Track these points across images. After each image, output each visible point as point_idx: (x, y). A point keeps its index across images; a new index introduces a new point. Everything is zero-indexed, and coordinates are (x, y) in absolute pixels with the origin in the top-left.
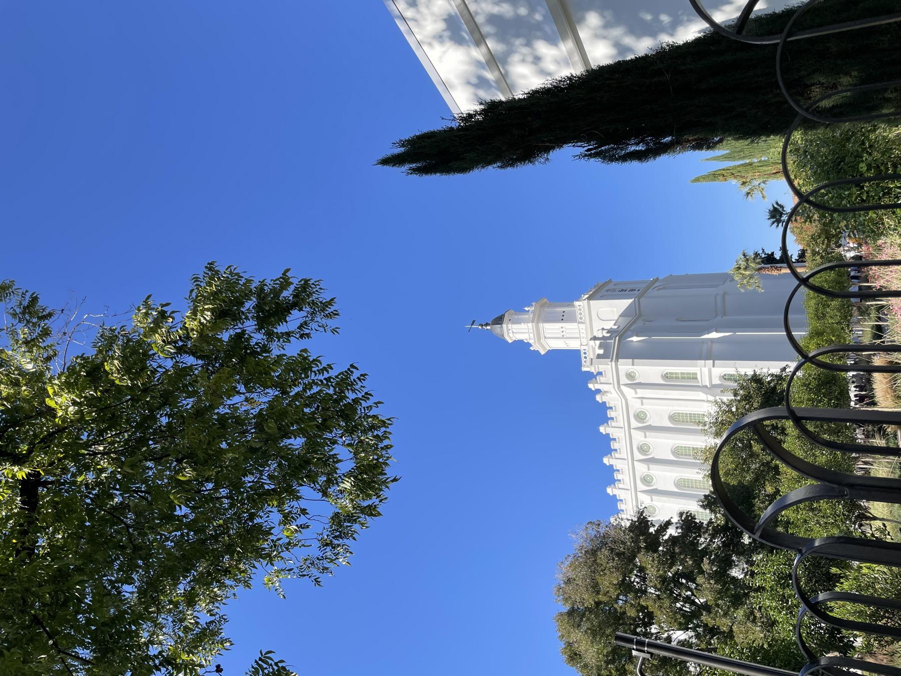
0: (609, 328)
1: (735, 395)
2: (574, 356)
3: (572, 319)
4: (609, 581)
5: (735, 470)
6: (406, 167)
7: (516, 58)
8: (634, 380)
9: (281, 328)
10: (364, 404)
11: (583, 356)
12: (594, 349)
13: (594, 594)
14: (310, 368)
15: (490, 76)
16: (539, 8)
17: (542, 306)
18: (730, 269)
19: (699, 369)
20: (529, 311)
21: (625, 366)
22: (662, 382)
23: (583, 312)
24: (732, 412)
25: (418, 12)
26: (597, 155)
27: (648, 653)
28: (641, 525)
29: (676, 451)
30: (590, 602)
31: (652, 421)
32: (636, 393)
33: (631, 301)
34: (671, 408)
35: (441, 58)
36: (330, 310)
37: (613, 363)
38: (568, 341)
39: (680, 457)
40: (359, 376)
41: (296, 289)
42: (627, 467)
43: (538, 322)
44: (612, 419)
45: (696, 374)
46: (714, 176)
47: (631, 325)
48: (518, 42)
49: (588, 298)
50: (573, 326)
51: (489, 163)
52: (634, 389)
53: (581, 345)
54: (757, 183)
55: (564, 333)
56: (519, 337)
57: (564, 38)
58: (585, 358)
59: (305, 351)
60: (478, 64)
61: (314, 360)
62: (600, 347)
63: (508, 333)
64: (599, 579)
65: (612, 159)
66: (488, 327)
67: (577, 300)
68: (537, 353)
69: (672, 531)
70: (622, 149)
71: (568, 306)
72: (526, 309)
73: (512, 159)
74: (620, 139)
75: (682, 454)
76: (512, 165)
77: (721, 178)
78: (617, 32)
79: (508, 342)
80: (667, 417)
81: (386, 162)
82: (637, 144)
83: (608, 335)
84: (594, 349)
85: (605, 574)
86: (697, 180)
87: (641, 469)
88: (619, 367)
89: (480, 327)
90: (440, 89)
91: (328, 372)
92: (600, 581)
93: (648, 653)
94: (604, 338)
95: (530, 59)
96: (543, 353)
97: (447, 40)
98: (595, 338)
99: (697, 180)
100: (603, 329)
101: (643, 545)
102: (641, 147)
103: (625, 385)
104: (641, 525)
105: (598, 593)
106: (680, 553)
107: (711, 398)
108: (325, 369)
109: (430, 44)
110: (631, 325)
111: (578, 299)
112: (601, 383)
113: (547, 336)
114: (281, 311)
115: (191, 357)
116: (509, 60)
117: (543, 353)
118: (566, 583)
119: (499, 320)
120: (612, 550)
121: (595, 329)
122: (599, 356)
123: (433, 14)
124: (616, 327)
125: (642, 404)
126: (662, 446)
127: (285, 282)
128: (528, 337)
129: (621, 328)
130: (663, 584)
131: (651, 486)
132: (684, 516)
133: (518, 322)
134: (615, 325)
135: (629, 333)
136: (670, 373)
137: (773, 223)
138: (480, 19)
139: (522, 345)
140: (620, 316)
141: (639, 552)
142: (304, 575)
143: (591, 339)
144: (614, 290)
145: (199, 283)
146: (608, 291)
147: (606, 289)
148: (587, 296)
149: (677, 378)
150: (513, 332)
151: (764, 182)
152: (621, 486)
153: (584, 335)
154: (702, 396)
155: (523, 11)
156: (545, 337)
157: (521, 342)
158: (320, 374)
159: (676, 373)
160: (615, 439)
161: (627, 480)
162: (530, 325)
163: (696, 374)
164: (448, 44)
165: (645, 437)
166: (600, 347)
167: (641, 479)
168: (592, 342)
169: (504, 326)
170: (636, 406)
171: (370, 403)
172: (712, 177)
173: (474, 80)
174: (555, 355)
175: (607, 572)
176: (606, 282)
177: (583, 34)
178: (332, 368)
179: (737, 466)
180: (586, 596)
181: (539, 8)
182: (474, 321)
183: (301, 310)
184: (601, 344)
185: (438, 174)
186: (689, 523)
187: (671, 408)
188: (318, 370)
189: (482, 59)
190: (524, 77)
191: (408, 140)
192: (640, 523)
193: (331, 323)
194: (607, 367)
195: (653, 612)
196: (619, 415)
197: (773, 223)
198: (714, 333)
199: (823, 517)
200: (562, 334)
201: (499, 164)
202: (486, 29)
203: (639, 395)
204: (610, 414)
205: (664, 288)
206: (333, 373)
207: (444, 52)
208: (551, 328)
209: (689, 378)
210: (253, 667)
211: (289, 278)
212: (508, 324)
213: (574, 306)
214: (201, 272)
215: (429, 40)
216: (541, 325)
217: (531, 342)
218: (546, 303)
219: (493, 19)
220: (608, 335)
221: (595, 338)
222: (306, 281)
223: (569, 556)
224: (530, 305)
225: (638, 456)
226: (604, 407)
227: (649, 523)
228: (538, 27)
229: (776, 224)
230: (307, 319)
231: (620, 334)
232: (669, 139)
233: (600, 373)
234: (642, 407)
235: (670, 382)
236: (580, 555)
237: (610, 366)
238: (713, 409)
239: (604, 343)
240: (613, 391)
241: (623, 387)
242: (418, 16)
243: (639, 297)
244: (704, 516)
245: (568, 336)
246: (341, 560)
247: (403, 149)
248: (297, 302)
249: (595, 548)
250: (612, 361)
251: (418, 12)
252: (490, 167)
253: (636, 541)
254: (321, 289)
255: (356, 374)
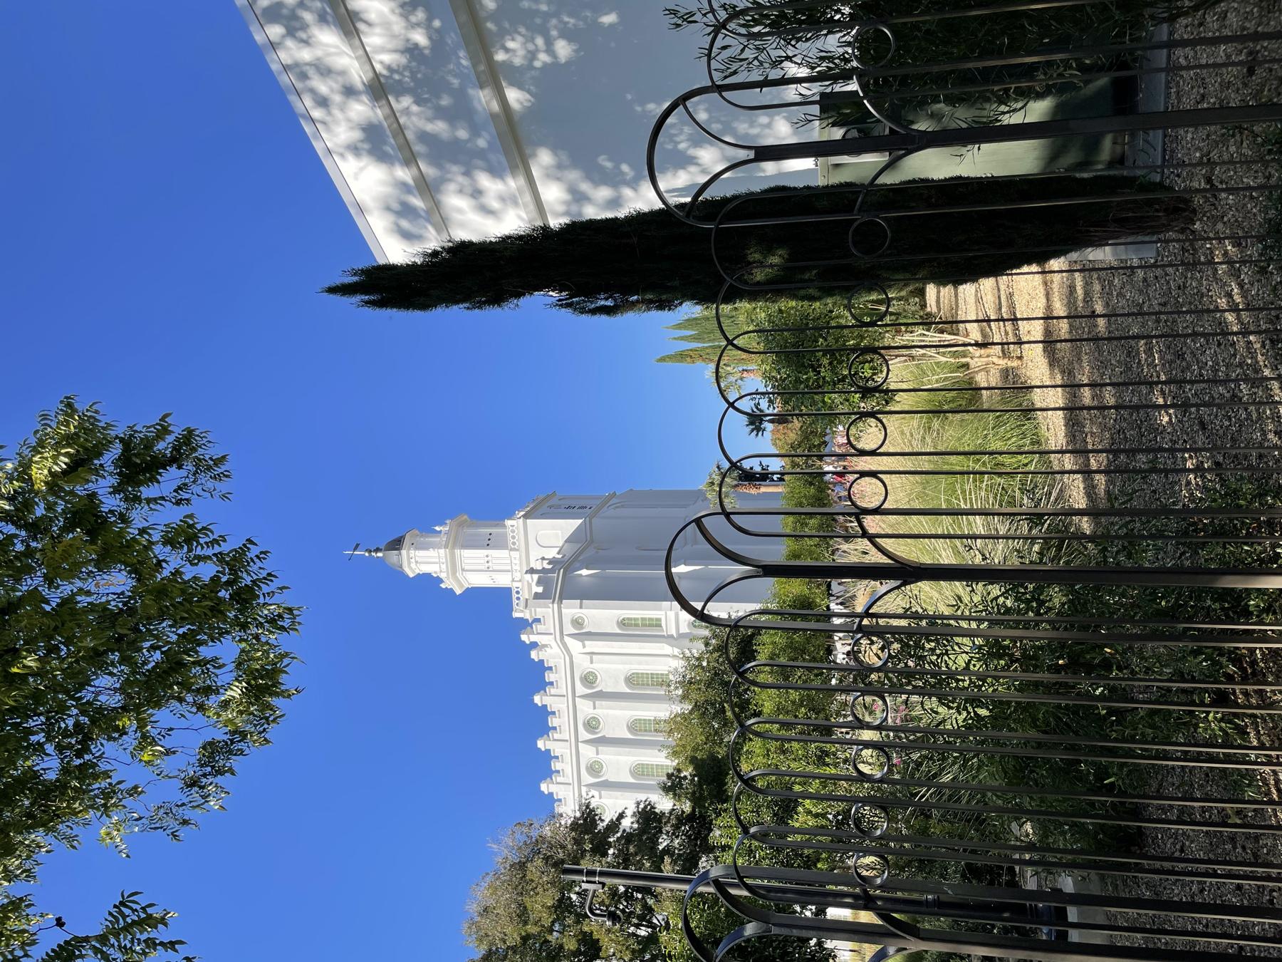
0: (551, 557)
1: (707, 644)
2: (501, 597)
3: (501, 544)
4: (541, 903)
5: (706, 744)
6: (358, 298)
7: (452, 187)
8: (582, 628)
9: (147, 492)
10: (265, 589)
11: (515, 596)
12: (530, 586)
13: (521, 925)
14: (195, 537)
15: (417, 202)
16: (484, 133)
17: (461, 525)
18: (702, 487)
19: (663, 613)
20: (440, 532)
21: (571, 609)
22: (618, 631)
23: (517, 528)
24: (703, 668)
25: (329, 113)
26: (569, 305)
27: (600, 883)
28: (588, 819)
29: (635, 726)
30: (514, 938)
31: (604, 685)
32: (584, 647)
33: (580, 521)
34: (628, 667)
35: (356, 176)
36: (220, 471)
37: (556, 605)
38: (495, 575)
39: (639, 733)
40: (258, 553)
41: (177, 439)
42: (568, 751)
43: (454, 547)
44: (551, 683)
45: (659, 620)
46: (682, 356)
47: (581, 553)
48: (455, 168)
49: (523, 516)
50: (503, 553)
51: (457, 302)
52: (582, 641)
53: (513, 580)
54: (734, 379)
55: (490, 564)
56: (425, 569)
57: (513, 169)
58: (518, 598)
59: (191, 516)
60: (403, 186)
61: (204, 528)
62: (539, 583)
63: (409, 563)
64: (528, 901)
65: (583, 311)
66: (380, 554)
67: (510, 518)
68: (450, 592)
69: (627, 823)
70: (592, 302)
71: (496, 526)
72: (437, 528)
73: (479, 302)
74: (589, 291)
75: (640, 730)
76: (480, 307)
77: (689, 359)
78: (573, 175)
79: (408, 576)
80: (623, 678)
81: (332, 290)
82: (606, 299)
83: (550, 567)
84: (530, 586)
85: (537, 894)
86: (662, 359)
87: (588, 752)
88: (564, 611)
89: (367, 554)
90: (352, 211)
91: (219, 545)
92: (528, 905)
93: (600, 883)
94: (544, 571)
95: (469, 190)
96: (458, 592)
97: (364, 153)
98: (532, 571)
99: (662, 359)
100: (543, 559)
101: (588, 847)
102: (610, 303)
103: (569, 635)
104: (588, 819)
105: (526, 923)
106: (636, 854)
107: (676, 651)
108: (215, 542)
109: (342, 155)
110: (581, 553)
111: (510, 516)
112: (538, 634)
113: (466, 568)
114: (153, 467)
115: (10, 526)
116: (442, 188)
117: (458, 592)
118: (481, 915)
119: (396, 544)
120: (546, 859)
121: (532, 559)
122: (537, 596)
123: (349, 120)
124: (560, 556)
125: (592, 662)
126: (616, 718)
127: (164, 431)
128: (438, 570)
129: (568, 556)
130: (613, 898)
131: (599, 777)
132: (642, 806)
133: (425, 547)
134: (558, 553)
135: (578, 565)
136: (628, 619)
137: (752, 431)
138: (410, 135)
139: (429, 582)
140: (566, 541)
141: (583, 857)
142: (156, 828)
143: (526, 573)
144: (559, 507)
145: (48, 422)
146: (550, 507)
147: (549, 504)
148: (522, 513)
149: (636, 625)
150: (417, 562)
151: (742, 379)
152: (560, 779)
153: (518, 568)
154: (667, 649)
155: (462, 134)
156: (463, 570)
157: (427, 576)
158: (208, 547)
159: (635, 619)
160: (554, 713)
161: (568, 770)
162: (442, 551)
163: (659, 620)
164: (365, 161)
165: (595, 708)
166: (539, 583)
167: (587, 768)
168: (528, 577)
169: (404, 552)
170: (583, 664)
171: (273, 586)
172: (679, 357)
173: (396, 206)
174: (474, 594)
175: (540, 890)
176: (548, 496)
177: (536, 172)
178: (225, 541)
179: (707, 739)
180: (508, 930)
181: (484, 133)
182: (358, 545)
183: (180, 467)
184: (539, 578)
185: (395, 310)
186: (648, 817)
187: (628, 667)
188: (206, 543)
189: (410, 182)
190: (460, 211)
191: (362, 270)
192: (585, 820)
193: (223, 486)
194: (546, 611)
195: (598, 940)
196: (561, 678)
197: (752, 431)
198: (683, 566)
199: (795, 760)
200: (486, 559)
201: (467, 305)
202: (418, 148)
203: (587, 650)
204: (550, 677)
205: (623, 506)
206: (225, 548)
207: (362, 169)
208: (471, 557)
209: (650, 625)
210: (110, 914)
211: (169, 425)
212: (409, 549)
213: (504, 526)
214: (55, 406)
215: (341, 150)
216: (457, 552)
217: (443, 576)
218: (466, 521)
219: (424, 137)
220: (550, 567)
221: (532, 571)
222: (190, 432)
223: (487, 874)
224: (442, 523)
225: (584, 735)
226: (541, 667)
227: (597, 818)
228: (481, 154)
229: (755, 432)
230: (187, 481)
231: (565, 565)
232: (636, 297)
233: (538, 620)
234: (591, 666)
235: (629, 630)
236: (503, 871)
237: (550, 610)
238: (679, 664)
239: (544, 577)
240: (554, 644)
241: (567, 639)
242: (328, 119)
243: (591, 517)
244: (664, 804)
245: (496, 568)
246: (212, 803)
247: (355, 279)
248: (176, 459)
249: (524, 860)
250: (553, 602)
251: (329, 113)
252: (455, 308)
253: (578, 842)
254: (210, 442)
255: (254, 551)
